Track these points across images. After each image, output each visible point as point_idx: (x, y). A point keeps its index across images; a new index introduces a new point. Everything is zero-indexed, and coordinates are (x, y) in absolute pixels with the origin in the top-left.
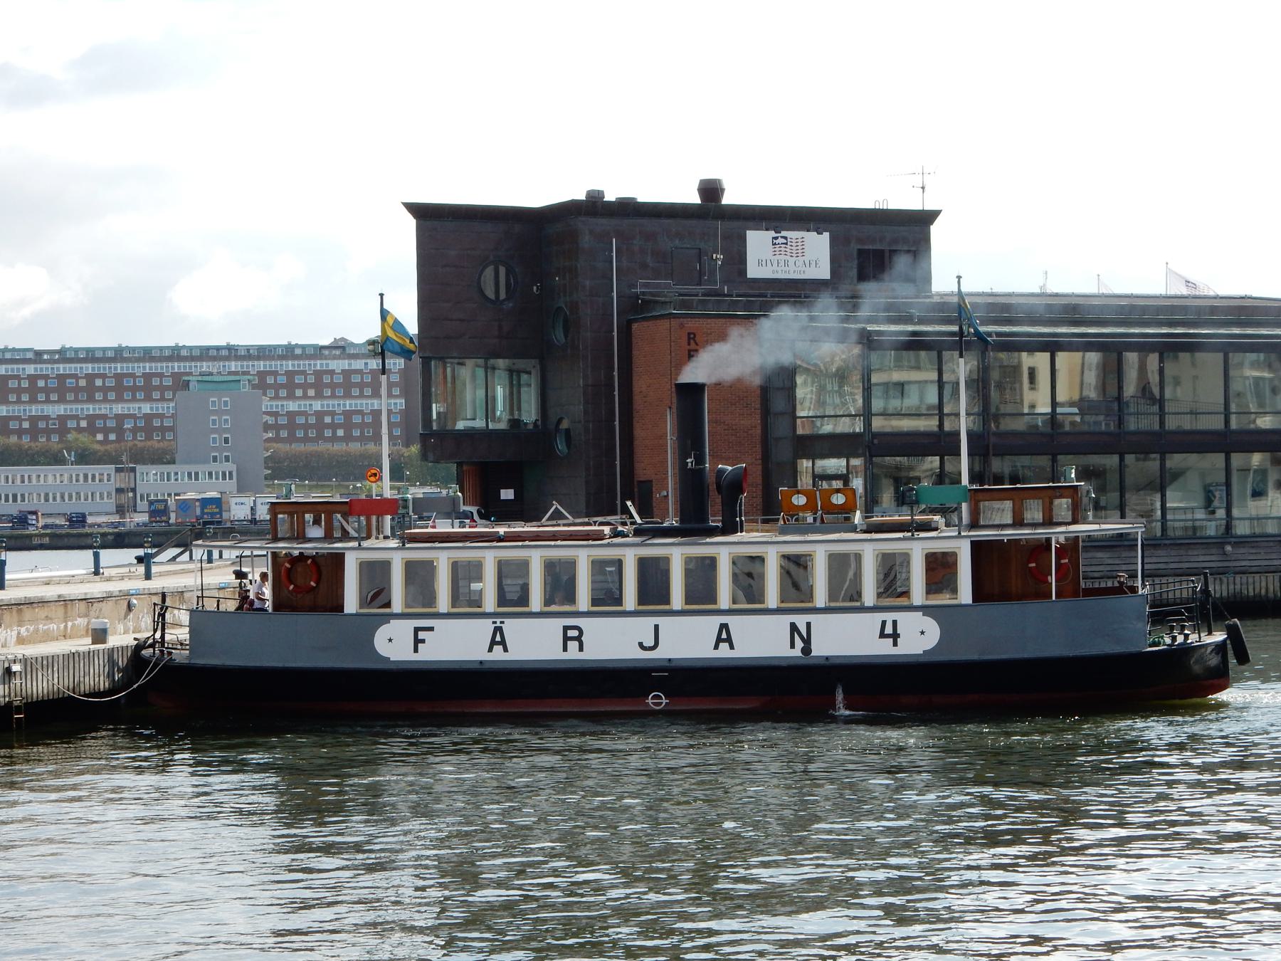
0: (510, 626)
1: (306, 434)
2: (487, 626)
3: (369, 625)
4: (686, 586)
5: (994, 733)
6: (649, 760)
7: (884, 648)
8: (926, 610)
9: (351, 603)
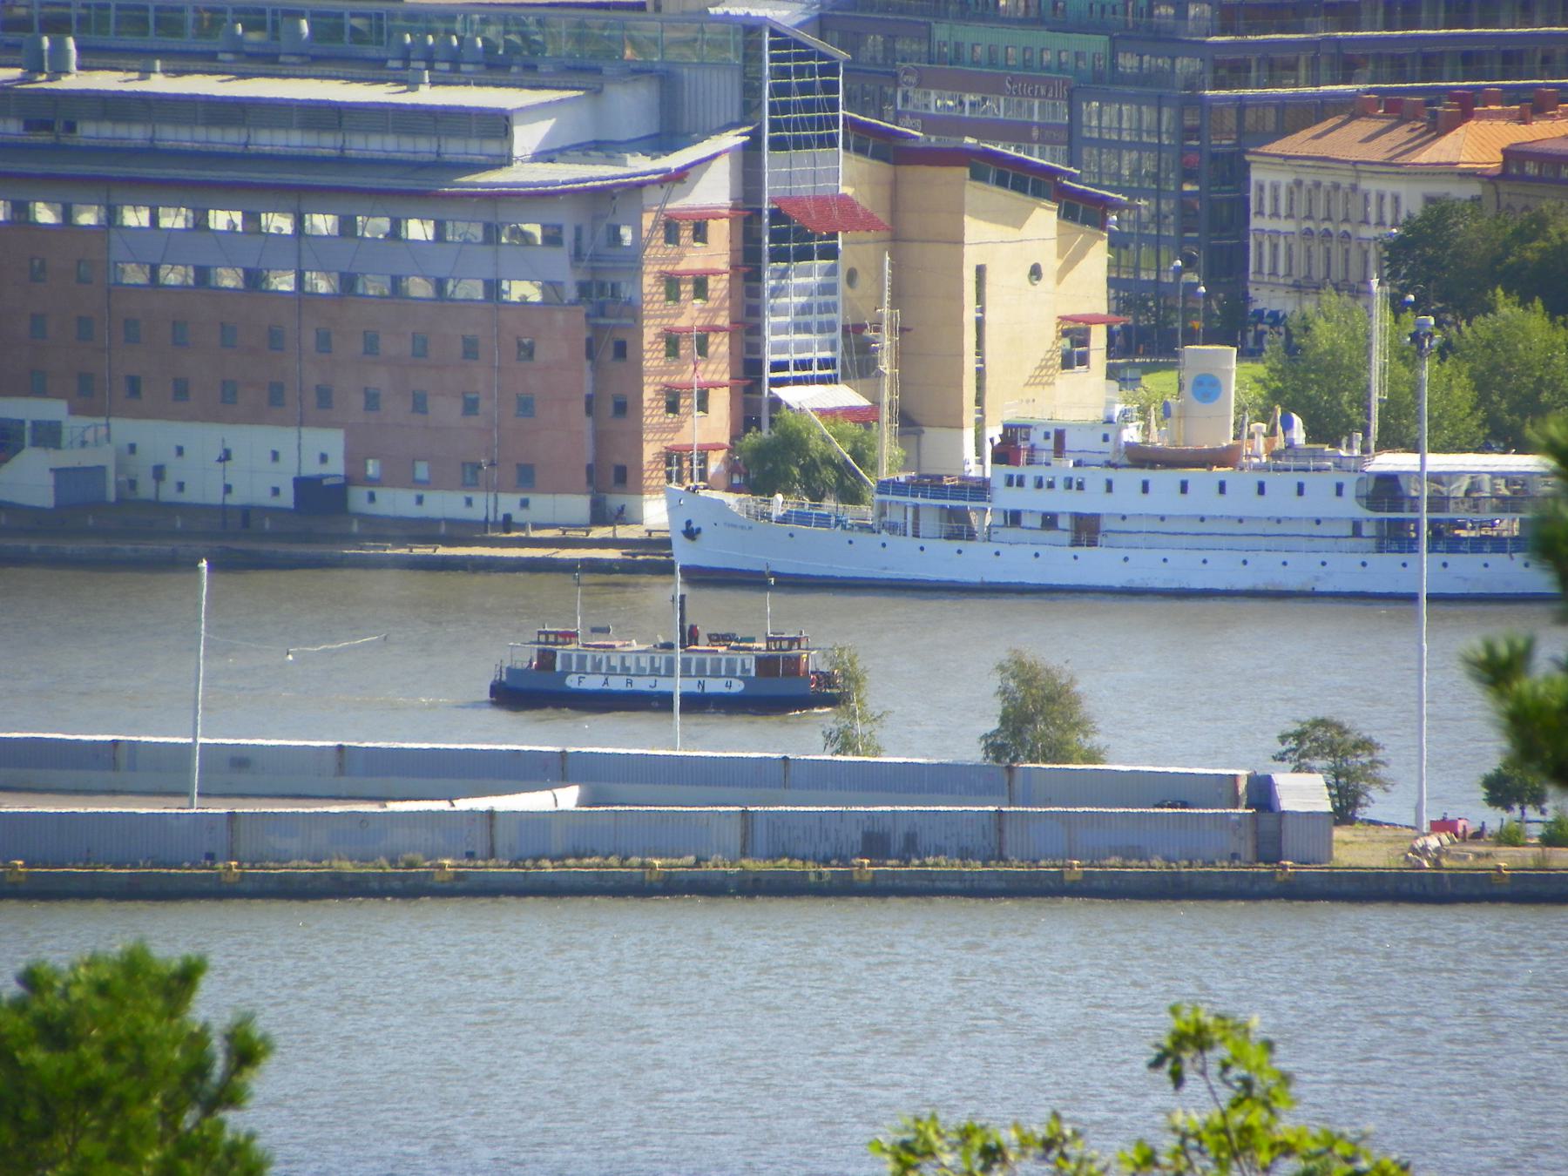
0: (611, 679)
1: (547, 638)
2: (602, 678)
3: (565, 674)
4: (346, 446)
5: (1230, 1141)
6: (1479, 1077)
7: (726, 690)
8: (740, 678)
9: (558, 667)
